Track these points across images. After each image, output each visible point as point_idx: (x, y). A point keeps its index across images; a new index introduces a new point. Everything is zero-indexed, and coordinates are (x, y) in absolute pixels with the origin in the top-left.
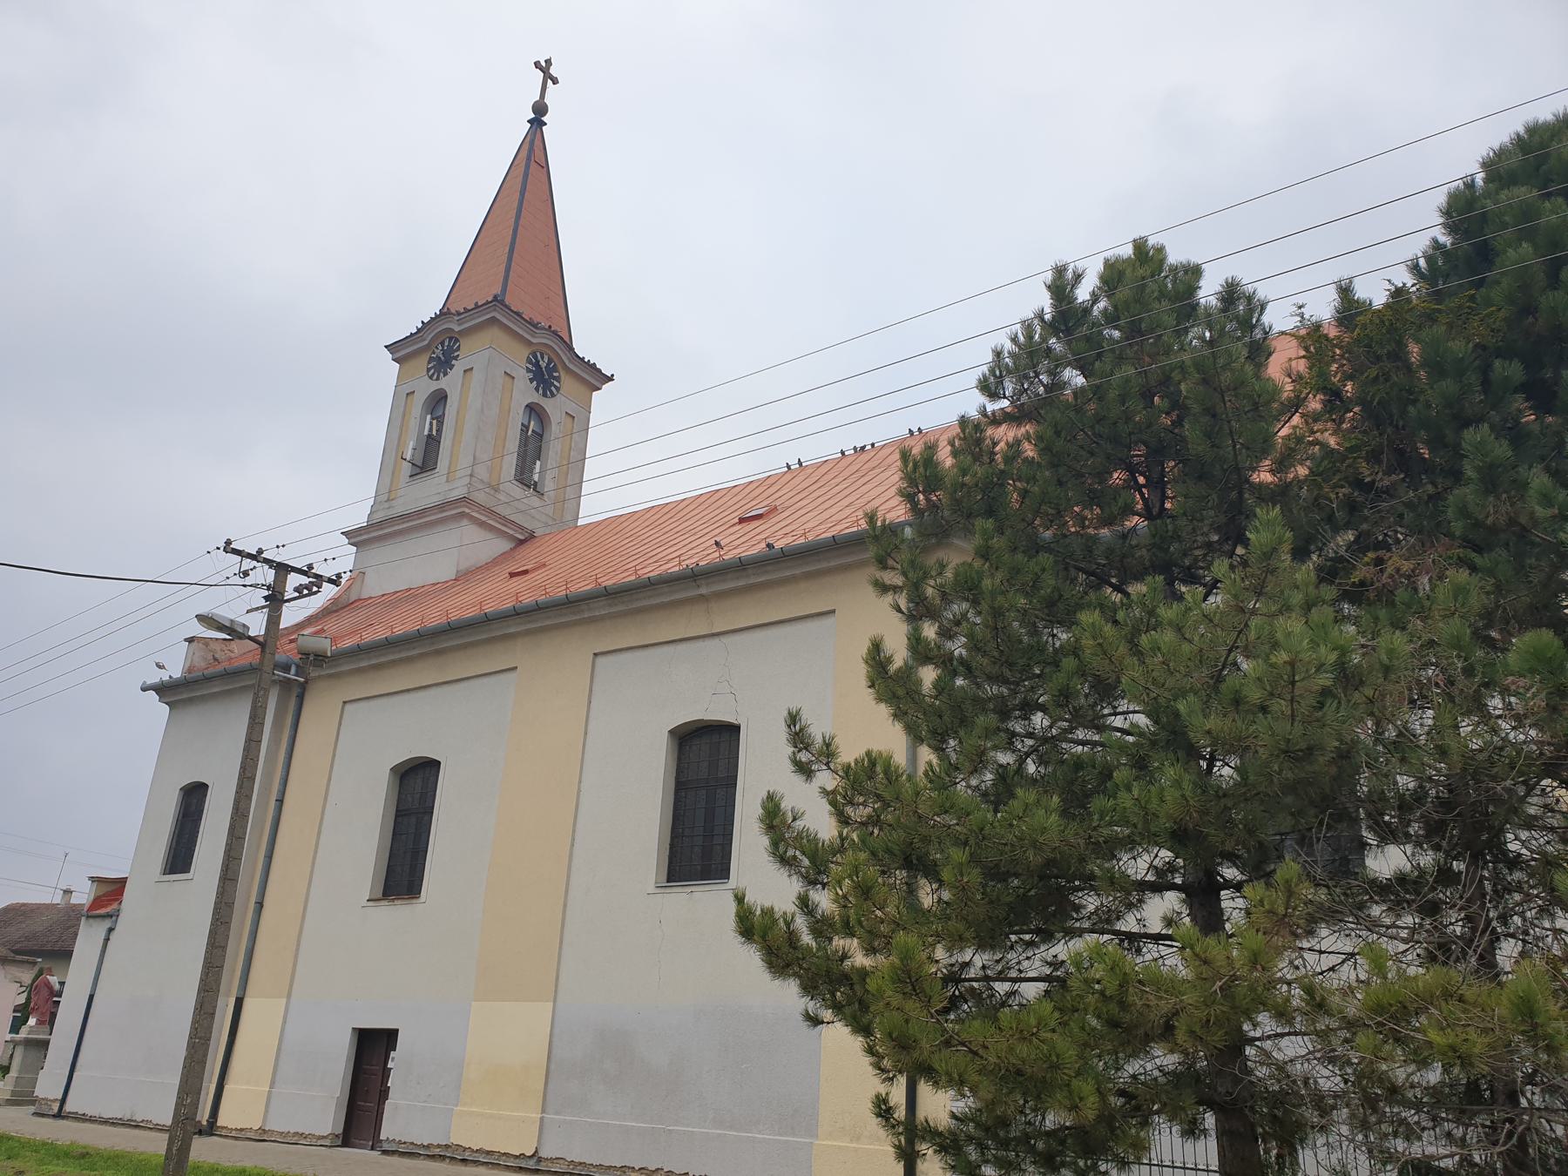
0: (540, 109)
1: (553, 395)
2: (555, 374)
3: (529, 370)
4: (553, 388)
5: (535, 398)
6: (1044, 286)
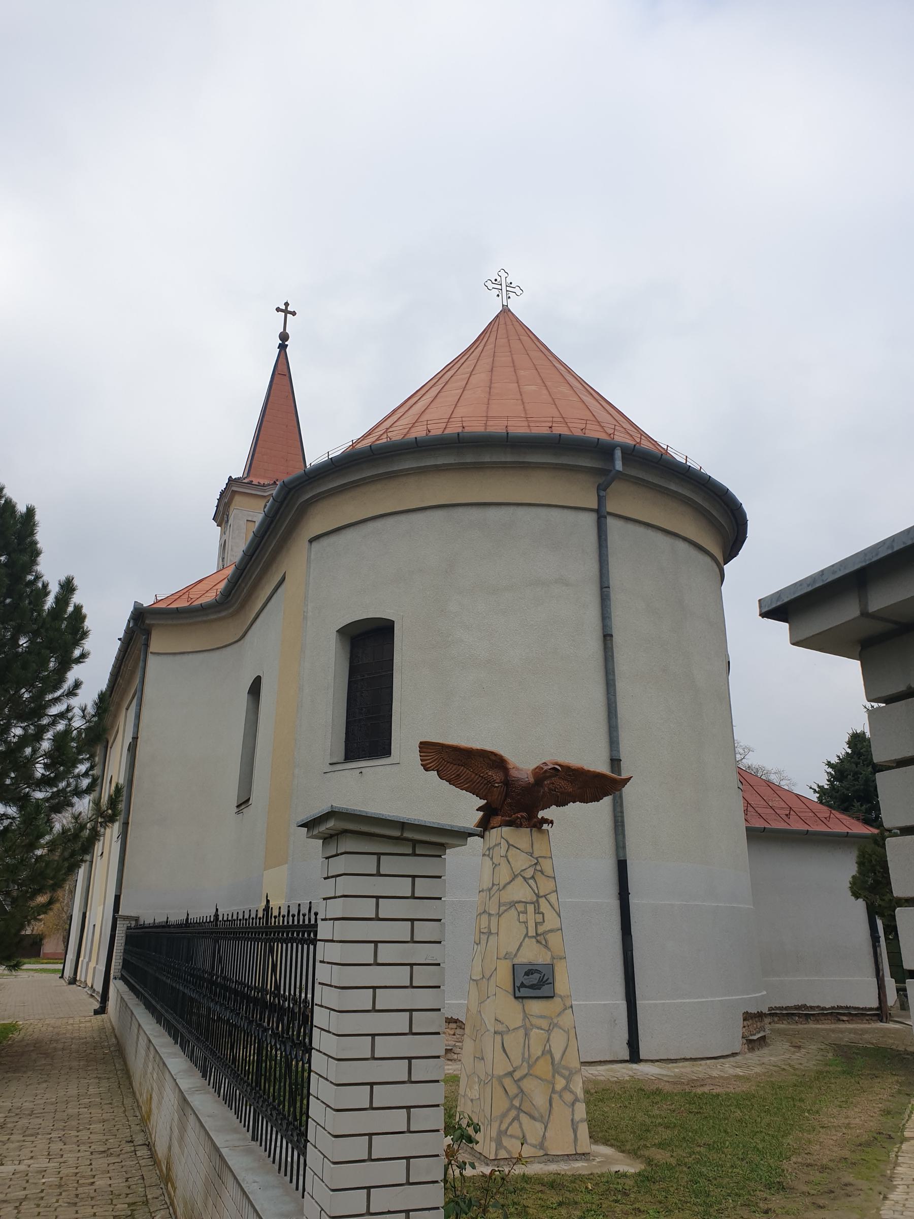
0: (284, 337)
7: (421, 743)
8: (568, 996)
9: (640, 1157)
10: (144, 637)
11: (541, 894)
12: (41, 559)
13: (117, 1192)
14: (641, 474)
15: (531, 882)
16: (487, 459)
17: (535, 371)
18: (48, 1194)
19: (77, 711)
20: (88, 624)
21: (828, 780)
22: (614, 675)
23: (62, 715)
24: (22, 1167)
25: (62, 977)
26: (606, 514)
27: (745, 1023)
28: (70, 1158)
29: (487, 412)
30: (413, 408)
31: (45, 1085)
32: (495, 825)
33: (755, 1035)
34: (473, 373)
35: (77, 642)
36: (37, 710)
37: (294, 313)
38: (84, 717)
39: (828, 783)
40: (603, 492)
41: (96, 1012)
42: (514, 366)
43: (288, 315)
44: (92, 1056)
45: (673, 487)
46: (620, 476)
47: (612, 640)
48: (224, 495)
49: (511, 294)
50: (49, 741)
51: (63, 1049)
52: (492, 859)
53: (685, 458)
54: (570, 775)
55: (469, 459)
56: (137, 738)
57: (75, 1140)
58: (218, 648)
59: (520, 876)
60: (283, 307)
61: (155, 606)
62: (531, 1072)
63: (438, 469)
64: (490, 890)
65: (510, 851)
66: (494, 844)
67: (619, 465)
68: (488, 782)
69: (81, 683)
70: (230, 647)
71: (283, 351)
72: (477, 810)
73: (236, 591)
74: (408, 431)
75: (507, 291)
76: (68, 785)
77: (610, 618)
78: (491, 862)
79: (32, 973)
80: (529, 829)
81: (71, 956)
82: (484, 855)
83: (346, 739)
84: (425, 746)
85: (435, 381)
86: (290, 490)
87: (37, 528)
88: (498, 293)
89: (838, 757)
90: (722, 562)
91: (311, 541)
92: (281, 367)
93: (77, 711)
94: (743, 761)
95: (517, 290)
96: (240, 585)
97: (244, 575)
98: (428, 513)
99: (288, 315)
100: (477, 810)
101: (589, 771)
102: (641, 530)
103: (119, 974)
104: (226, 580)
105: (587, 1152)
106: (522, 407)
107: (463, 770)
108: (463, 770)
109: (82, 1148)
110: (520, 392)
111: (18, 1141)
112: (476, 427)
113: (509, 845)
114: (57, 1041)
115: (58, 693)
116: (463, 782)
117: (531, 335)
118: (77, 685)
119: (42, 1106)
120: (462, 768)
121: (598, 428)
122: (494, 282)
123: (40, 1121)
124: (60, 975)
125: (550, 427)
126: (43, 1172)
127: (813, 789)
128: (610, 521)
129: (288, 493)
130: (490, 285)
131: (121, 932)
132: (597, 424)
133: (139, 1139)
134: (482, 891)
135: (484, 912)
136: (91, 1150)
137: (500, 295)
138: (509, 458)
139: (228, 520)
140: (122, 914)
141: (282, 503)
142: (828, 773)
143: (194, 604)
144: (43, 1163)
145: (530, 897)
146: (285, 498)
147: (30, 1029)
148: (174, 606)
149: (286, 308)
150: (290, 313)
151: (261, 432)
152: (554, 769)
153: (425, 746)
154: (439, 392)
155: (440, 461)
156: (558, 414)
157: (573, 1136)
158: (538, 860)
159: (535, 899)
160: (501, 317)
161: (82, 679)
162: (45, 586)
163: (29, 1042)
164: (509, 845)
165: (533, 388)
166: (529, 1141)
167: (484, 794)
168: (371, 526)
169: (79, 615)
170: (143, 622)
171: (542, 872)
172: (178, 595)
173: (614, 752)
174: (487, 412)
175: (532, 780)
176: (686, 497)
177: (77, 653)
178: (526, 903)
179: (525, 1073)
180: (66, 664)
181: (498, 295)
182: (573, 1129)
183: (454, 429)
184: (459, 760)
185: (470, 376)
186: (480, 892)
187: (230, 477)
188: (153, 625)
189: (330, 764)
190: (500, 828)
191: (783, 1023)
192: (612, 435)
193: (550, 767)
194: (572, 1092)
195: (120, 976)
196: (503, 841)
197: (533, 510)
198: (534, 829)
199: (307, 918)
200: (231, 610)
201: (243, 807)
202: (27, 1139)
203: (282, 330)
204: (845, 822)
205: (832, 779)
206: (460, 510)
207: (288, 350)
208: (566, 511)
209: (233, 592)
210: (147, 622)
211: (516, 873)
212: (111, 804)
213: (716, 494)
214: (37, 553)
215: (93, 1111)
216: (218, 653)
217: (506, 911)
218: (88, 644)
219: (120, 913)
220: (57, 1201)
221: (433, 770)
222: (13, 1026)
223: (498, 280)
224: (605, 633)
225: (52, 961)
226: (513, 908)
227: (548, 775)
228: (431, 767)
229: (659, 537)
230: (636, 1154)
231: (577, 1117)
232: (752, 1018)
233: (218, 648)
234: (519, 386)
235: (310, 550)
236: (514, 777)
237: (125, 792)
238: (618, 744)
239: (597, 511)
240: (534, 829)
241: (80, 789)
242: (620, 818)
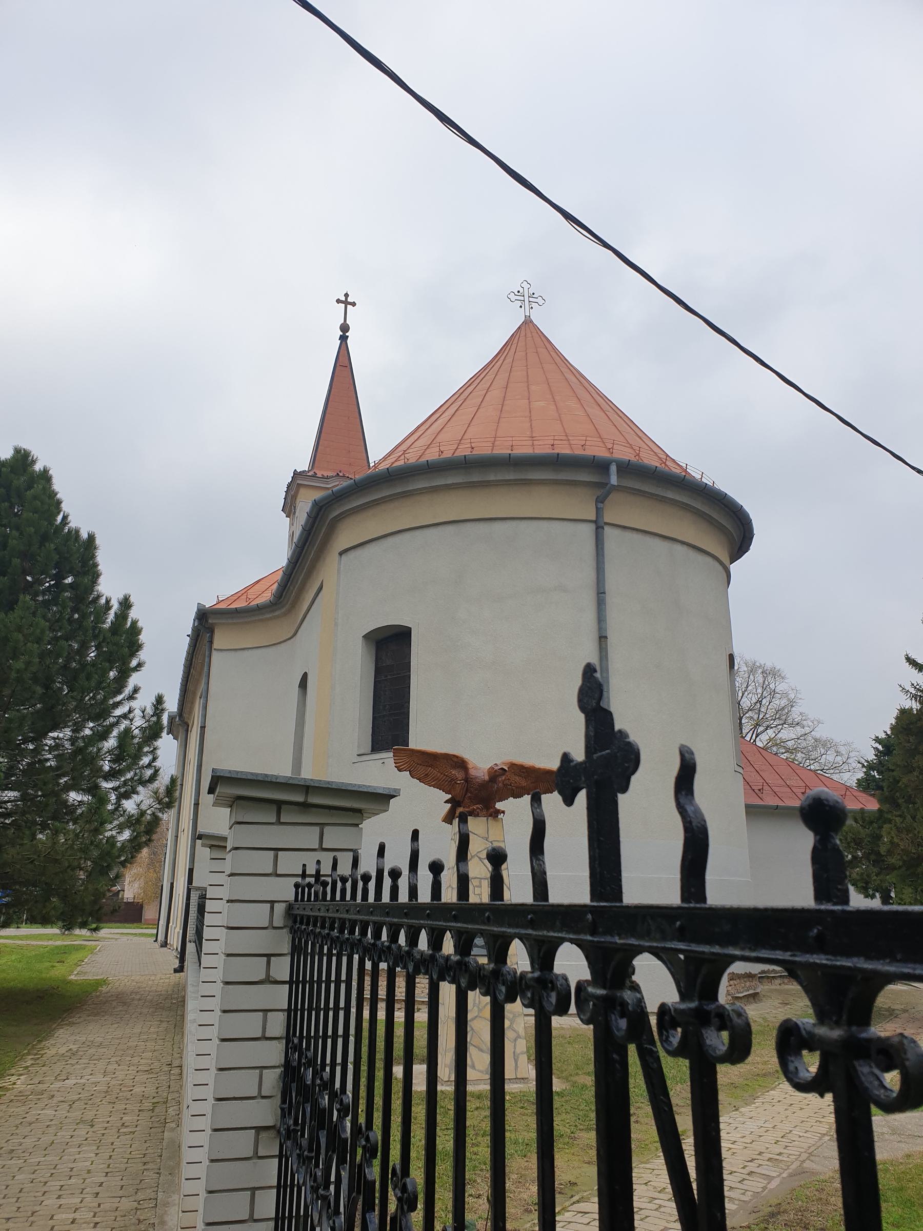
0: (345, 328)
8: (514, 955)
9: (569, 1081)
10: (208, 635)
12: (101, 580)
13: (147, 1096)
14: (637, 485)
16: (492, 477)
18: (96, 1097)
19: (138, 713)
20: (142, 638)
21: (876, 755)
23: (125, 716)
24: (83, 1081)
25: (156, 941)
27: (732, 982)
28: (120, 1075)
30: (432, 426)
31: (116, 1026)
33: (742, 993)
34: (489, 390)
35: (133, 654)
36: (101, 712)
37: (354, 304)
38: (144, 717)
39: (876, 758)
40: (600, 504)
41: (176, 971)
42: (528, 382)
43: (348, 306)
44: (161, 1005)
48: (290, 487)
49: (533, 305)
50: (115, 739)
51: (140, 1000)
54: (523, 772)
55: (476, 477)
56: (205, 727)
57: (128, 1063)
58: (274, 645)
59: (476, 857)
60: (343, 299)
62: (480, 1015)
67: (614, 480)
69: (140, 688)
71: (344, 342)
72: (445, 802)
73: (287, 592)
74: (424, 452)
76: (135, 774)
79: (131, 937)
81: (162, 922)
82: (452, 839)
85: (457, 396)
87: (97, 551)
88: (520, 304)
89: (885, 732)
91: (341, 554)
92: (343, 361)
93: (138, 713)
94: (812, 733)
95: (540, 300)
96: (289, 587)
97: (291, 579)
98: (440, 528)
99: (348, 306)
100: (445, 802)
101: (539, 769)
104: (277, 584)
105: (526, 1077)
109: (132, 1068)
111: (85, 1064)
112: (484, 449)
114: (137, 993)
115: (119, 698)
118: (136, 690)
119: (110, 1040)
120: (430, 768)
122: (517, 293)
123: (105, 1050)
124: (155, 939)
126: (96, 1084)
127: (861, 764)
133: (176, 1063)
136: (138, 1069)
137: (523, 306)
139: (295, 512)
141: (316, 518)
142: (874, 748)
143: (251, 604)
144: (99, 1078)
146: (318, 514)
147: (117, 984)
148: (233, 606)
149: (346, 299)
150: (351, 304)
151: (325, 424)
152: (502, 769)
154: (457, 410)
155: (449, 481)
157: (514, 1065)
160: (523, 328)
161: (139, 685)
162: (108, 601)
163: (113, 994)
165: (542, 404)
166: (477, 1068)
168: (390, 540)
169: (135, 630)
170: (207, 621)
172: (237, 596)
176: (683, 503)
177: (134, 663)
178: (481, 879)
179: (475, 1015)
180: (125, 673)
181: (521, 307)
182: (515, 1059)
183: (464, 451)
187: (295, 470)
189: (358, 755)
191: (793, 984)
194: (515, 1031)
197: (535, 523)
198: (490, 818)
199: (449, 879)
200: (283, 610)
202: (91, 1062)
203: (343, 322)
204: (860, 800)
205: (878, 754)
206: (469, 525)
207: (348, 341)
208: (566, 523)
210: (210, 621)
211: (473, 855)
212: (167, 794)
213: (716, 499)
214: (97, 575)
215: (147, 1044)
216: (274, 648)
218: (143, 655)
219: (193, 885)
220: (101, 1101)
221: (405, 770)
222: (104, 981)
223: (521, 292)
225: (151, 926)
229: (657, 542)
230: (567, 1079)
231: (518, 1051)
232: (739, 978)
233: (274, 645)
234: (529, 402)
237: (179, 783)
239: (595, 522)
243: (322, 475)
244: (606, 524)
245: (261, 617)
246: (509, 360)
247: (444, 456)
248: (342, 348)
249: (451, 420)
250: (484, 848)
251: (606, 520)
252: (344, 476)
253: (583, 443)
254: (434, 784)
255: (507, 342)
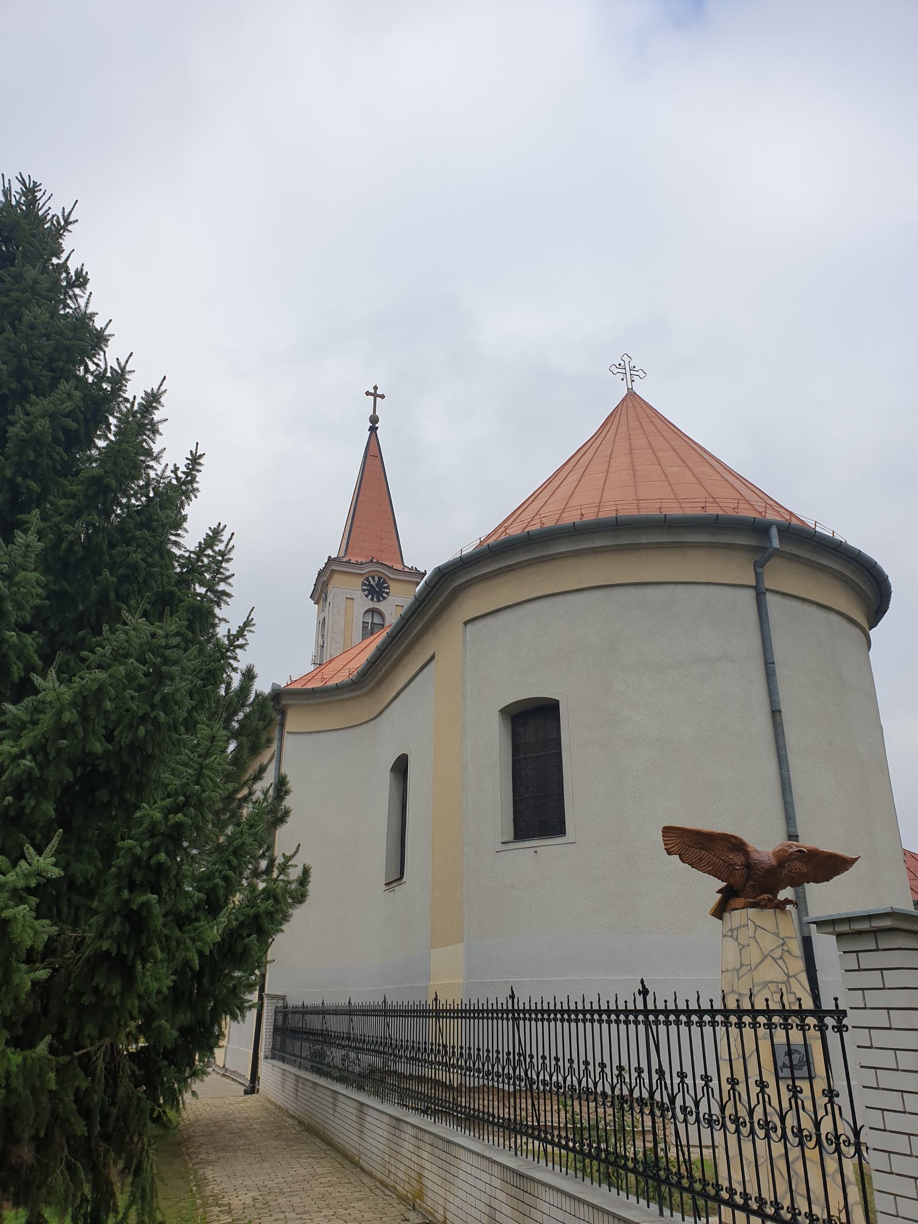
0: (374, 420)
1: (384, 598)
2: (385, 585)
3: (364, 590)
4: (384, 595)
5: (372, 605)
6: (96, 312)
7: (664, 828)
11: (791, 974)
14: (795, 551)
15: (780, 962)
16: (644, 540)
17: (673, 452)
22: (786, 750)
26: (764, 590)
29: (636, 494)
32: (737, 907)
37: (382, 397)
42: (652, 448)
45: (825, 562)
46: (776, 553)
47: (781, 716)
48: (323, 574)
52: (737, 939)
53: (832, 533)
55: (626, 540)
58: (352, 727)
60: (372, 391)
61: (290, 687)
63: (594, 551)
64: (738, 970)
65: (757, 932)
66: (738, 925)
67: (776, 543)
68: (729, 864)
70: (364, 725)
71: (374, 433)
72: (717, 892)
74: (560, 516)
75: (631, 375)
77: (777, 693)
78: (736, 943)
80: (773, 910)
83: (514, 818)
84: (668, 831)
86: (444, 575)
90: (867, 628)
91: (465, 624)
95: (641, 373)
97: (382, 656)
100: (717, 892)
102: (797, 604)
103: (270, 1053)
106: (669, 488)
107: (705, 853)
108: (705, 853)
110: (664, 474)
112: (629, 510)
113: (756, 926)
116: (705, 866)
117: (661, 417)
120: (704, 851)
121: (748, 506)
122: (618, 366)
125: (703, 508)
128: (769, 597)
129: (441, 578)
130: (615, 370)
131: (270, 1011)
132: (745, 502)
134: (727, 971)
135: (731, 992)
137: (625, 379)
138: (665, 539)
140: (269, 993)
143: (327, 684)
145: (781, 977)
148: (309, 686)
149: (375, 391)
153: (668, 831)
155: (597, 544)
156: (706, 495)
158: (784, 940)
159: (786, 979)
164: (756, 926)
167: (726, 876)
171: (788, 952)
173: (792, 828)
174: (636, 494)
175: (774, 863)
181: (623, 379)
184: (700, 843)
185: (610, 459)
186: (722, 972)
187: (330, 557)
188: (288, 705)
189: (502, 843)
190: (745, 910)
192: (736, 509)
193: (795, 850)
195: (270, 1056)
196: (750, 923)
200: (365, 690)
201: (394, 885)
206: (619, 589)
208: (724, 588)
209: (369, 672)
210: (283, 702)
211: (765, 954)
216: (352, 730)
217: (760, 991)
221: (675, 854)
224: (773, 709)
226: (766, 989)
227: (794, 857)
228: (673, 851)
229: (814, 610)
233: (352, 727)
235: (465, 632)
236: (756, 860)
238: (795, 819)
239: (756, 588)
240: (777, 910)
241: (260, 870)
242: (802, 895)
243: (356, 561)
244: (767, 590)
245: (339, 698)
246: (613, 431)
247: (585, 519)
248: (372, 439)
249: (579, 486)
250: (775, 946)
251: (767, 586)
252: (378, 562)
253: (736, 505)
254: (711, 870)
255: (612, 414)
